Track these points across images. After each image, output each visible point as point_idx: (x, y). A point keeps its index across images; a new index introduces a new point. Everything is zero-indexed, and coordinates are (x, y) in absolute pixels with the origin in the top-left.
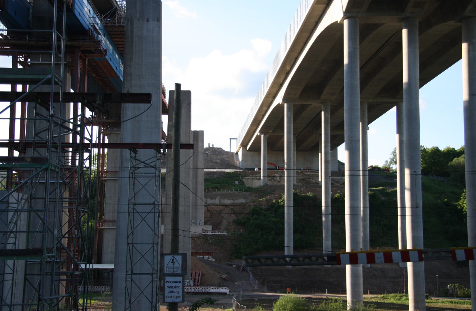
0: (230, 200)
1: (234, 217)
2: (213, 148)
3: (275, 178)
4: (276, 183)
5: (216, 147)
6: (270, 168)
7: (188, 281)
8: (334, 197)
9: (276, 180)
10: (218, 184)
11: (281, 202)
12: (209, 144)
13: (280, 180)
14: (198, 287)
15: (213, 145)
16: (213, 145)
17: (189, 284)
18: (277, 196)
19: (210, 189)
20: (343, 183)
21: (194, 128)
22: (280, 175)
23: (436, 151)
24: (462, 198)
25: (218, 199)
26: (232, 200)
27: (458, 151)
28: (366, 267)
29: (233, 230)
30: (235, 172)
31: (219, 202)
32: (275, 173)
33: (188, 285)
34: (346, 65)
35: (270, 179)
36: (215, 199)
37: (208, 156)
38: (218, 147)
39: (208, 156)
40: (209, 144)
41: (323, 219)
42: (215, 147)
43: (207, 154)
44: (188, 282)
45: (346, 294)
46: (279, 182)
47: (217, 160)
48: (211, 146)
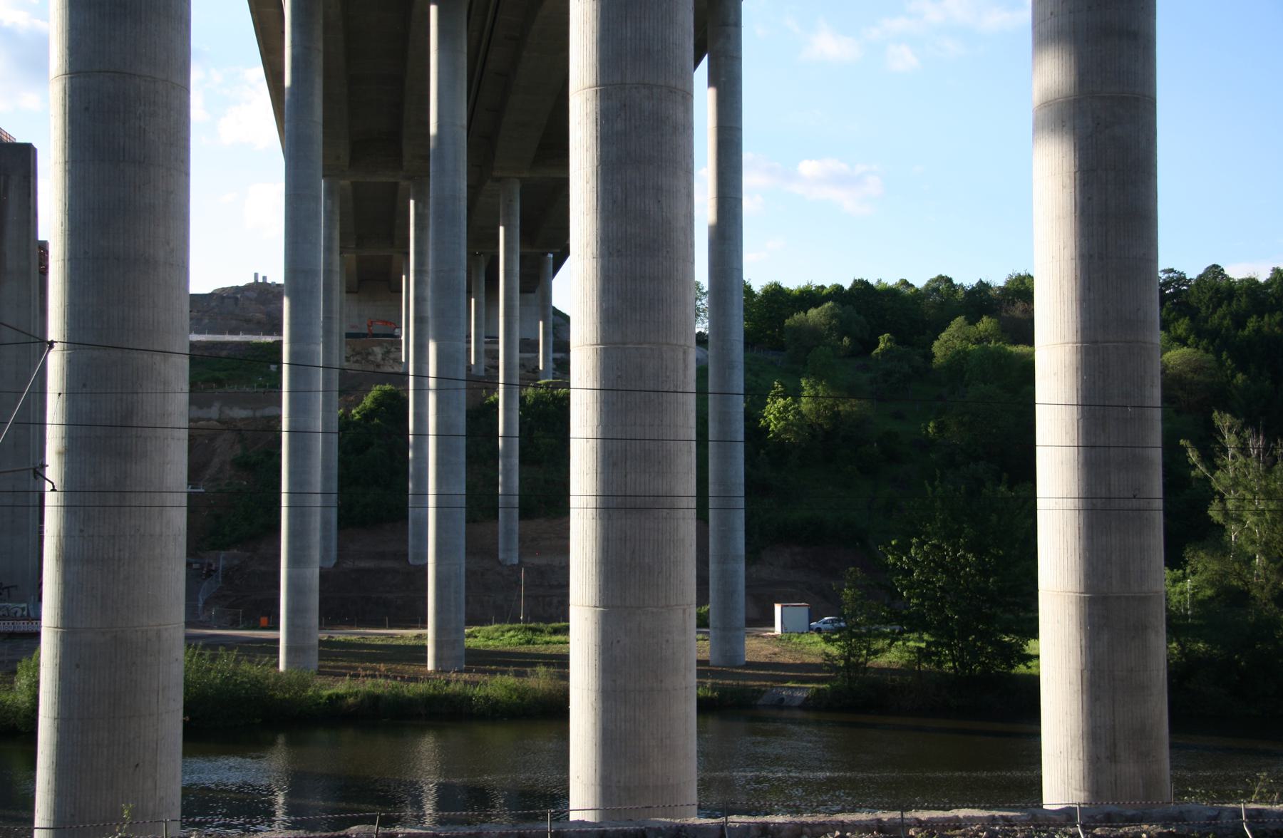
0: (245, 409)
1: (238, 450)
2: (265, 284)
3: (371, 358)
4: (372, 368)
5: (273, 283)
6: (386, 332)
7: (24, 605)
8: (487, 401)
9: (373, 362)
10: (225, 370)
11: (357, 415)
12: (256, 275)
13: (382, 363)
14: (4, 620)
15: (264, 278)
16: (264, 278)
17: (25, 613)
18: (352, 401)
19: (199, 383)
20: (534, 367)
21: (41, 237)
22: (385, 350)
23: (776, 294)
24: (769, 400)
25: (217, 406)
26: (252, 408)
27: (922, 289)
28: (509, 564)
29: (227, 481)
30: (275, 341)
31: (220, 415)
32: (374, 346)
33: (22, 616)
34: (288, 88)
35: (359, 359)
36: (210, 406)
37: (236, 304)
38: (277, 283)
39: (236, 304)
40: (256, 275)
41: (411, 455)
42: (269, 281)
43: (237, 298)
44: (23, 609)
45: (426, 628)
46: (378, 366)
47: (257, 314)
48: (260, 280)
